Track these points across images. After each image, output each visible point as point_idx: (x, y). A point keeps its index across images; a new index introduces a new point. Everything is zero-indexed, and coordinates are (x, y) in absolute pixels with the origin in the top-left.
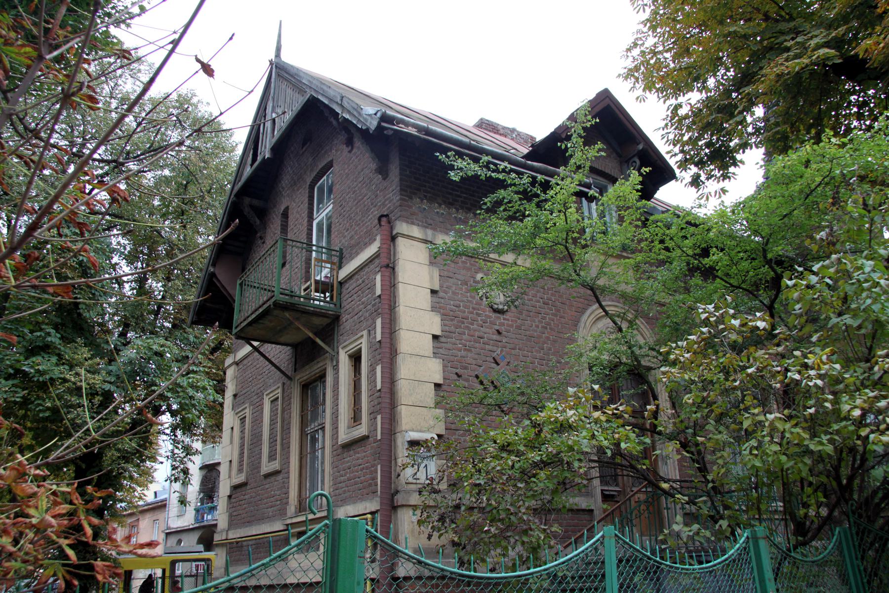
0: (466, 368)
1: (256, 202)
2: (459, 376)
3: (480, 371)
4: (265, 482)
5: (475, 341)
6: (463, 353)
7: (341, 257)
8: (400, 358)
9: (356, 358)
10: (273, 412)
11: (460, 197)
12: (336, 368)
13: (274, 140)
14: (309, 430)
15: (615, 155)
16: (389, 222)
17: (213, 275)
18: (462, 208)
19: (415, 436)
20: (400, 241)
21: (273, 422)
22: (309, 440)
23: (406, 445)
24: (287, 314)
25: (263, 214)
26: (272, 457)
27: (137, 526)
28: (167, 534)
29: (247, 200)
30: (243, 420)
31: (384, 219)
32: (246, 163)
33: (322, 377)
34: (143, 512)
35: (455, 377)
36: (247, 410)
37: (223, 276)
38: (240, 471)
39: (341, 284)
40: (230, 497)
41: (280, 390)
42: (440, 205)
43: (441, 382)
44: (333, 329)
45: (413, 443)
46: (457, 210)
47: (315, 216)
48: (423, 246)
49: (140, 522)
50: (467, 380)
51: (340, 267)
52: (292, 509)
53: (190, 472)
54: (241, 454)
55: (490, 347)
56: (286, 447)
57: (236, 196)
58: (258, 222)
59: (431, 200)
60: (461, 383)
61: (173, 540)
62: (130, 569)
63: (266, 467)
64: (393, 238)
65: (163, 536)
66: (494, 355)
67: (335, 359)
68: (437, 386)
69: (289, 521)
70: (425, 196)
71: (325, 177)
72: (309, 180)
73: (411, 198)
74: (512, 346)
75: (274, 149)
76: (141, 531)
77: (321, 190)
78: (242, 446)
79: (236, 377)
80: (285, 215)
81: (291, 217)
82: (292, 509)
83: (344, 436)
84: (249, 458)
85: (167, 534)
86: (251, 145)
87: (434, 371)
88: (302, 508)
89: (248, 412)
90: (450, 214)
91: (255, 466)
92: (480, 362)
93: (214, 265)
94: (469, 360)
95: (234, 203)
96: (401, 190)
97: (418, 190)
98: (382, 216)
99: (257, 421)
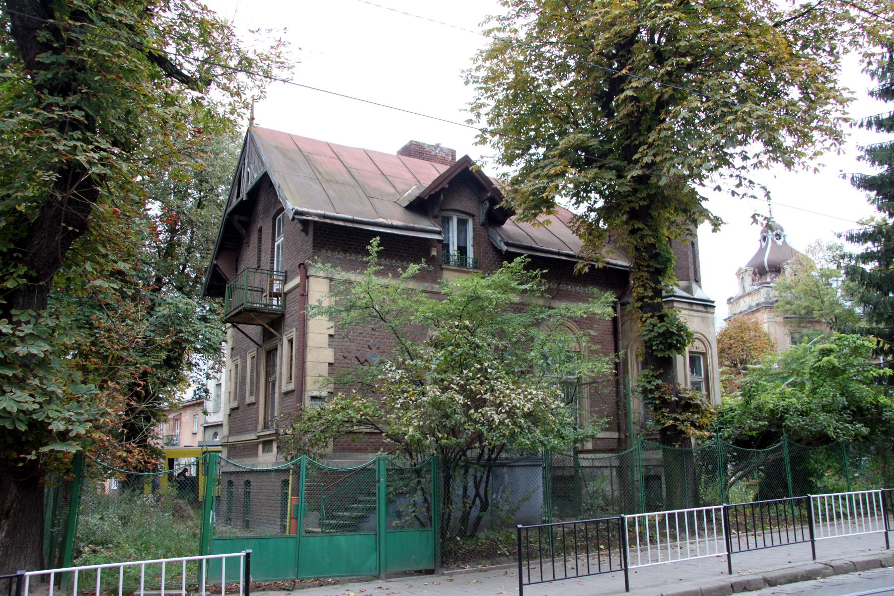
0: (350, 352)
1: (243, 218)
2: (345, 358)
3: (358, 354)
4: (248, 408)
5: (357, 336)
6: (348, 343)
7: (286, 277)
8: (308, 349)
9: (291, 341)
10: (252, 364)
11: (353, 245)
12: (282, 346)
13: (249, 188)
14: (270, 380)
15: (475, 197)
16: (305, 268)
17: (216, 266)
18: (354, 253)
19: (316, 393)
20: (311, 279)
21: (252, 372)
22: (270, 385)
23: (309, 399)
24: (252, 315)
25: (248, 226)
26: (251, 394)
27: (180, 419)
28: (205, 428)
29: (236, 217)
30: (237, 366)
31: (302, 266)
32: (233, 194)
33: (276, 349)
34: (185, 407)
35: (343, 358)
36: (239, 360)
37: (223, 267)
38: (235, 399)
39: (286, 294)
40: (230, 415)
41: (255, 352)
42: (339, 252)
43: (333, 362)
44: (281, 321)
45: (313, 398)
46: (351, 254)
47: (276, 239)
48: (326, 280)
49: (183, 415)
50: (350, 360)
51: (285, 283)
52: (260, 427)
53: (210, 391)
54: (236, 388)
55: (367, 339)
56: (258, 388)
57: (228, 215)
58: (244, 232)
59: (333, 250)
60: (346, 361)
61: (210, 432)
62: (172, 457)
63: (249, 399)
64: (308, 277)
65: (202, 429)
66: (369, 344)
67: (281, 340)
68: (330, 364)
69: (258, 434)
70: (330, 248)
71: (281, 215)
72: (273, 214)
73: (320, 250)
74: (382, 337)
75: (248, 194)
76: (183, 425)
77: (279, 220)
78: (236, 383)
79: (233, 336)
80: (260, 230)
81: (263, 231)
82: (260, 427)
83: (285, 388)
84: (240, 391)
85: (205, 428)
86: (236, 182)
87: (329, 355)
88: (266, 427)
89: (239, 362)
90: (345, 257)
91: (243, 397)
92: (359, 348)
93: (216, 259)
94: (352, 347)
95: (227, 219)
96: (314, 246)
97: (325, 244)
98: (301, 264)
99: (244, 368)
